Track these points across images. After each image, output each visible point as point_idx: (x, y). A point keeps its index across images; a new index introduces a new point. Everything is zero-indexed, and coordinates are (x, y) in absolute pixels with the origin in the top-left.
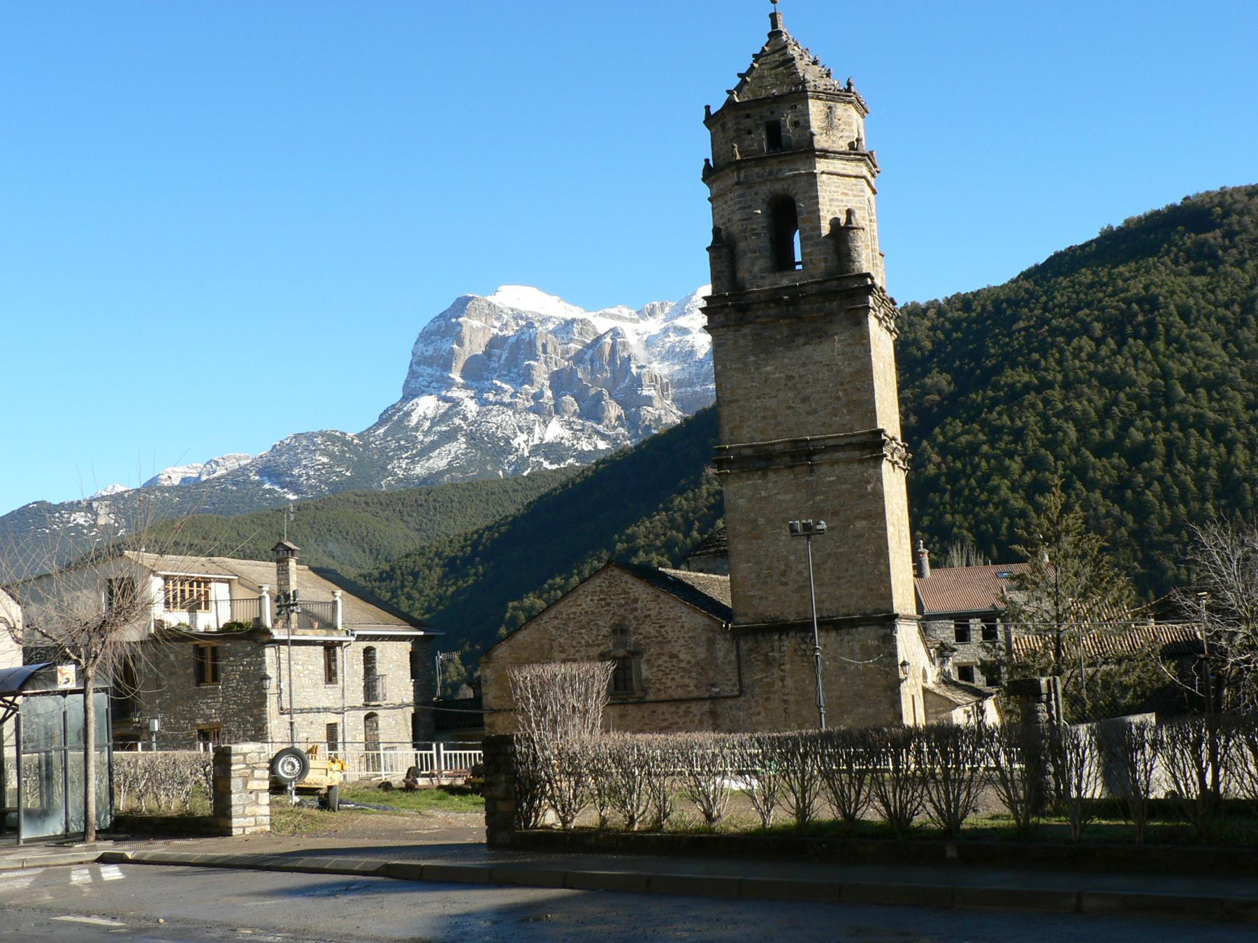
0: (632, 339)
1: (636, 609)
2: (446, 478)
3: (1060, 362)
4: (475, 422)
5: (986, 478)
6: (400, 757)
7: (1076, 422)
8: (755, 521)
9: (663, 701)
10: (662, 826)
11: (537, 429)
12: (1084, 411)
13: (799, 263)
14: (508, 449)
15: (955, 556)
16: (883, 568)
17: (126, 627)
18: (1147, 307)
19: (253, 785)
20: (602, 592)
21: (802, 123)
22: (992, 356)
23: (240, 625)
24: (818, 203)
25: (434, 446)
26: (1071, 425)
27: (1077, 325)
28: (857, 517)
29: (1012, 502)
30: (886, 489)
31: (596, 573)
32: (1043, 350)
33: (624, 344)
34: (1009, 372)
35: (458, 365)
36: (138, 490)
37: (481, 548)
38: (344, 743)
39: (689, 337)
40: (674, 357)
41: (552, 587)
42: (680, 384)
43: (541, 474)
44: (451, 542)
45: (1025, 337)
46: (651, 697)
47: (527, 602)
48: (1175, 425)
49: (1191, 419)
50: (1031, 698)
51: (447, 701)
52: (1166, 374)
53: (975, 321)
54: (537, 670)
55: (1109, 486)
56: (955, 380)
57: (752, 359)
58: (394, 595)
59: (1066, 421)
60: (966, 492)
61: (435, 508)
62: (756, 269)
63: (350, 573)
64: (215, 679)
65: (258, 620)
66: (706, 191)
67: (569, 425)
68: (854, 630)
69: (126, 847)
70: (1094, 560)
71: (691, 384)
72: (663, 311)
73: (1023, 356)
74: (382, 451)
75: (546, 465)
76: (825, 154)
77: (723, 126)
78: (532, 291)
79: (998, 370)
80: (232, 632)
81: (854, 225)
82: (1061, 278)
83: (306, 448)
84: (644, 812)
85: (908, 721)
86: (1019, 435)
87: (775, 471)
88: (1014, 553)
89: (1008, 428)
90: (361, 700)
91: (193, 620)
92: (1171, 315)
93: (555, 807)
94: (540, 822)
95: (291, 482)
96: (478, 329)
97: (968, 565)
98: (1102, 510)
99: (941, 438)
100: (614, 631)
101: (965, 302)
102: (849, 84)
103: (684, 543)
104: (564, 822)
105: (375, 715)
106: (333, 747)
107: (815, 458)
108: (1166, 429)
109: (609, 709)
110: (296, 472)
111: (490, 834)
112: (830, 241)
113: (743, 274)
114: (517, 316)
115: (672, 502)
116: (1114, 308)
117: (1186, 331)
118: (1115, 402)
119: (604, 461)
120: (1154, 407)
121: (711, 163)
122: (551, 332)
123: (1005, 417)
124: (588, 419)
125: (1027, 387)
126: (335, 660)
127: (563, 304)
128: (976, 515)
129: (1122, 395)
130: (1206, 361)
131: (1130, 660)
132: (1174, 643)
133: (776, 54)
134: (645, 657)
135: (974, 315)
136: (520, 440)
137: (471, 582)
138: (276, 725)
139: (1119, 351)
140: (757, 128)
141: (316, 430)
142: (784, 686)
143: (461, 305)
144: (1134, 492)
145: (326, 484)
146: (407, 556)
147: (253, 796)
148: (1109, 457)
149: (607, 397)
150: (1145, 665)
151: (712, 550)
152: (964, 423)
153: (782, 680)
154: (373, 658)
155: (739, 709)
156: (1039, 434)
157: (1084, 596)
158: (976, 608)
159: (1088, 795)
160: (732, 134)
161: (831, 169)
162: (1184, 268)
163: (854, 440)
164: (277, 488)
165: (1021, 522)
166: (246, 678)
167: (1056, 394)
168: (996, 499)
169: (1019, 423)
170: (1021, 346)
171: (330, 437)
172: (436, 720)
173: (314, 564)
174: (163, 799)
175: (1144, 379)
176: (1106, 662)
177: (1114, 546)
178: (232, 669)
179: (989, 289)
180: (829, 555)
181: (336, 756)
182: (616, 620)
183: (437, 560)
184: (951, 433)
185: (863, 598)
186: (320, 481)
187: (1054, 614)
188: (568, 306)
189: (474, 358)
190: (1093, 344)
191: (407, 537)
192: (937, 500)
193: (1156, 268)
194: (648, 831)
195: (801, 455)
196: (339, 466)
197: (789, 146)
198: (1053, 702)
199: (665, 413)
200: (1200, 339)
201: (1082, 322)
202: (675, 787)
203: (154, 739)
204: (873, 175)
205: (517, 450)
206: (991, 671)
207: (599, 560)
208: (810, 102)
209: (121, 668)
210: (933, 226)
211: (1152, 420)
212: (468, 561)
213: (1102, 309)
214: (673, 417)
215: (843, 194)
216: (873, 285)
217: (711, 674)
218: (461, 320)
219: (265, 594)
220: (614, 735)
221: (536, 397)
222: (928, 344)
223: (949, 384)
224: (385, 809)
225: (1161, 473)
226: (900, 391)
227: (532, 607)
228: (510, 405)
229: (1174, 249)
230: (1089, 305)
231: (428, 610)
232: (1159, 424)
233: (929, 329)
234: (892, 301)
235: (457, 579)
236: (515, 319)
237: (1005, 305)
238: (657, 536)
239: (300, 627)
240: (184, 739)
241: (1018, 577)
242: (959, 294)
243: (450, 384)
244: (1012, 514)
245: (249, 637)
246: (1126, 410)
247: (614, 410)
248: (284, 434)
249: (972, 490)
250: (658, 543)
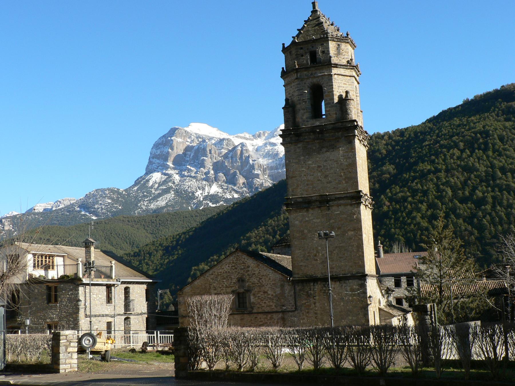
0: (250, 148)
1: (249, 271)
2: (165, 210)
3: (444, 160)
4: (178, 185)
5: (410, 212)
6: (140, 337)
7: (451, 187)
8: (303, 231)
9: (260, 313)
10: (254, 369)
11: (207, 188)
12: (455, 183)
13: (324, 115)
14: (193, 197)
15: (395, 247)
16: (360, 253)
17: (13, 277)
18: (484, 135)
19: (70, 350)
20: (233, 262)
21: (326, 52)
22: (413, 157)
23: (68, 276)
24: (333, 88)
25: (159, 195)
26: (449, 189)
27: (452, 144)
28: (349, 230)
29: (422, 223)
30: (362, 217)
31: (231, 254)
32: (437, 155)
33: (247, 150)
34: (421, 165)
35: (171, 159)
36: (23, 214)
37: (180, 242)
38: (114, 331)
39: (276, 147)
40: (269, 156)
41: (212, 260)
42: (271, 168)
43: (207, 209)
44: (167, 239)
45: (428, 149)
46: (255, 311)
47: (201, 267)
48: (496, 189)
49: (504, 187)
50: (423, 313)
51: (162, 312)
52: (492, 166)
53: (406, 141)
54: (199, 298)
55: (467, 217)
56: (396, 168)
57: (302, 158)
58: (140, 263)
59: (447, 187)
60: (401, 219)
61: (160, 224)
62: (304, 117)
63: (120, 253)
64: (56, 301)
65: (76, 274)
66: (282, 82)
67: (221, 186)
68: (347, 282)
69: (10, 378)
70: (457, 251)
71: (277, 169)
72: (264, 135)
73: (427, 157)
74: (136, 197)
75: (210, 204)
76: (336, 66)
77: (290, 53)
78: (205, 126)
79: (416, 163)
80: (64, 279)
81: (349, 98)
82: (445, 122)
83: (101, 196)
84: (246, 364)
85: (372, 323)
86: (425, 193)
87: (313, 209)
88: (422, 247)
89: (421, 190)
90: (123, 312)
91: (47, 274)
92: (495, 139)
93: (206, 360)
94: (199, 368)
95: (94, 211)
96: (180, 143)
97: (401, 252)
98: (463, 228)
99: (390, 194)
100: (239, 281)
101: (401, 133)
102: (347, 34)
103: (273, 241)
104: (210, 367)
105: (129, 318)
106: (109, 332)
107: (330, 203)
108: (493, 191)
109: (231, 317)
110: (96, 206)
111: (176, 372)
112: (338, 105)
113: (299, 119)
114: (198, 137)
115: (267, 222)
116: (470, 136)
117: (502, 147)
118: (469, 178)
119: (237, 203)
120: (487, 181)
121: (285, 69)
122: (213, 144)
123: (419, 185)
124: (230, 184)
125: (429, 172)
126: (111, 293)
127: (219, 132)
128: (405, 229)
129: (472, 176)
130: (511, 160)
131: (474, 296)
132: (495, 289)
133: (315, 21)
134: (253, 292)
135: (405, 138)
136: (199, 193)
137: (175, 257)
138: (84, 323)
139: (471, 156)
140: (306, 54)
141: (106, 187)
142: (315, 306)
143: (173, 132)
144: (477, 220)
145: (110, 212)
146: (147, 245)
147: (70, 355)
148: (466, 204)
149: (238, 174)
150: (481, 299)
151: (284, 244)
152: (401, 187)
153: (315, 304)
154: (129, 292)
155: (295, 317)
156: (434, 193)
157: (452, 267)
158: (404, 272)
159: (444, 358)
160: (294, 56)
161: (339, 73)
162: (502, 118)
163: (348, 195)
164: (87, 214)
165: (426, 233)
166: (70, 300)
167: (442, 175)
168: (415, 222)
169: (425, 188)
170: (427, 153)
171: (112, 191)
172: (156, 321)
173: (104, 249)
174: (29, 356)
175: (482, 169)
176: (462, 297)
177: (466, 244)
178: (64, 297)
179: (412, 127)
180: (336, 247)
181: (110, 336)
182: (239, 276)
183: (160, 247)
184: (394, 192)
185: (351, 267)
186: (107, 211)
187: (439, 275)
188: (221, 132)
189: (178, 156)
190: (459, 152)
191: (146, 237)
192: (388, 222)
193: (488, 118)
194: (247, 371)
195: (324, 201)
196: (116, 204)
197: (320, 62)
198: (433, 315)
199: (265, 181)
200: (508, 150)
201: (454, 142)
202: (259, 352)
203: (27, 328)
204: (358, 76)
205: (197, 198)
206: (410, 300)
207: (234, 248)
208: (330, 42)
209: (10, 296)
210: (387, 97)
211: (486, 187)
212: (174, 248)
213: (464, 136)
214: (269, 184)
215: (344, 84)
216: (357, 125)
217: (282, 300)
218: (172, 138)
219: (79, 262)
220: (233, 328)
221: (207, 173)
222: (384, 152)
223: (394, 170)
224: (131, 361)
225: (490, 211)
226: (369, 173)
227: (203, 269)
228: (194, 177)
229: (497, 109)
230: (458, 134)
231: (156, 270)
232: (490, 189)
233: (385, 145)
234: (366, 132)
235: (169, 256)
236: (197, 138)
237: (419, 134)
238: (260, 237)
239: (95, 278)
240: (41, 328)
241: (423, 258)
242: (398, 129)
243: (167, 167)
244: (421, 229)
245: (72, 282)
246: (474, 182)
247: (241, 180)
248: (91, 189)
249: (404, 218)
250: (261, 241)
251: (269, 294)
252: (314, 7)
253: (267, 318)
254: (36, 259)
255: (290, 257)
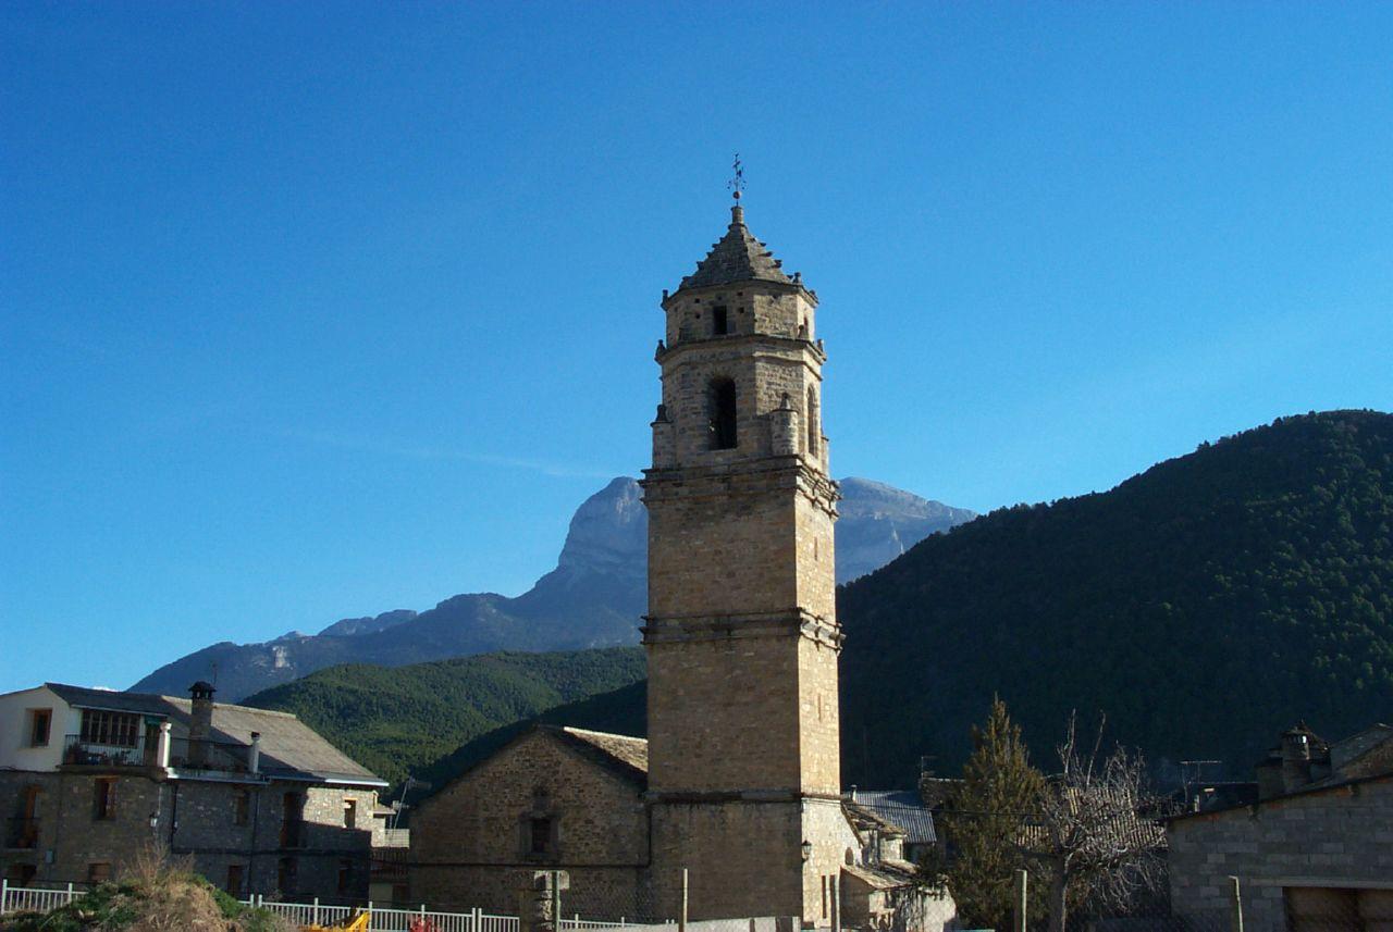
66: (658, 370)
100: (535, 794)
121: (665, 344)
134: (563, 820)
185: (772, 774)
195: (723, 628)
251: (597, 827)
252: (735, 218)
253: (587, 878)
254: (91, 722)
255: (645, 741)
